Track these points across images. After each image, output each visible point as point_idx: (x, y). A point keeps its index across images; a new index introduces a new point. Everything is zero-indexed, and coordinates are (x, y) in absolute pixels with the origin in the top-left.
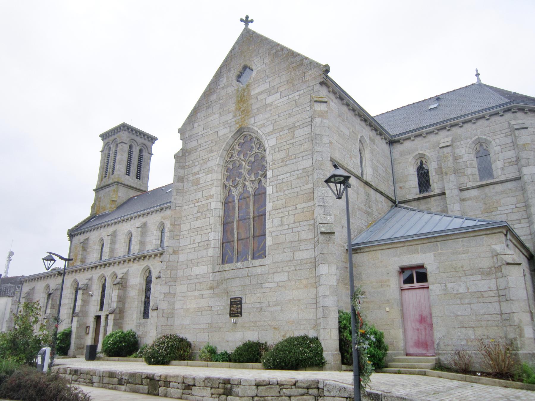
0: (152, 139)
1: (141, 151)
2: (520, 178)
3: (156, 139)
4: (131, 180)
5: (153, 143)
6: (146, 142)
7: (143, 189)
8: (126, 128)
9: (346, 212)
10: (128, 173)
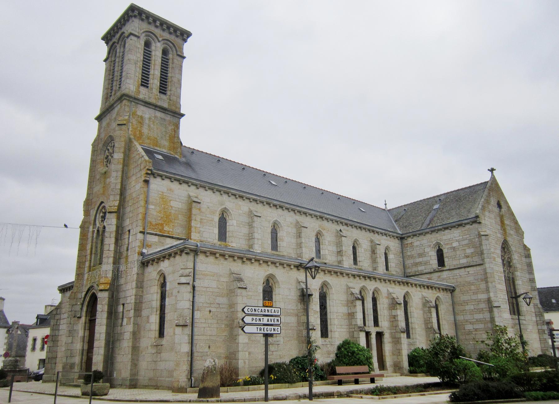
0: (184, 35)
1: (165, 52)
2: (482, 264)
3: (189, 34)
4: (151, 93)
5: (185, 41)
6: (172, 38)
7: (173, 108)
8: (136, 13)
9: (362, 320)
10: (145, 83)
